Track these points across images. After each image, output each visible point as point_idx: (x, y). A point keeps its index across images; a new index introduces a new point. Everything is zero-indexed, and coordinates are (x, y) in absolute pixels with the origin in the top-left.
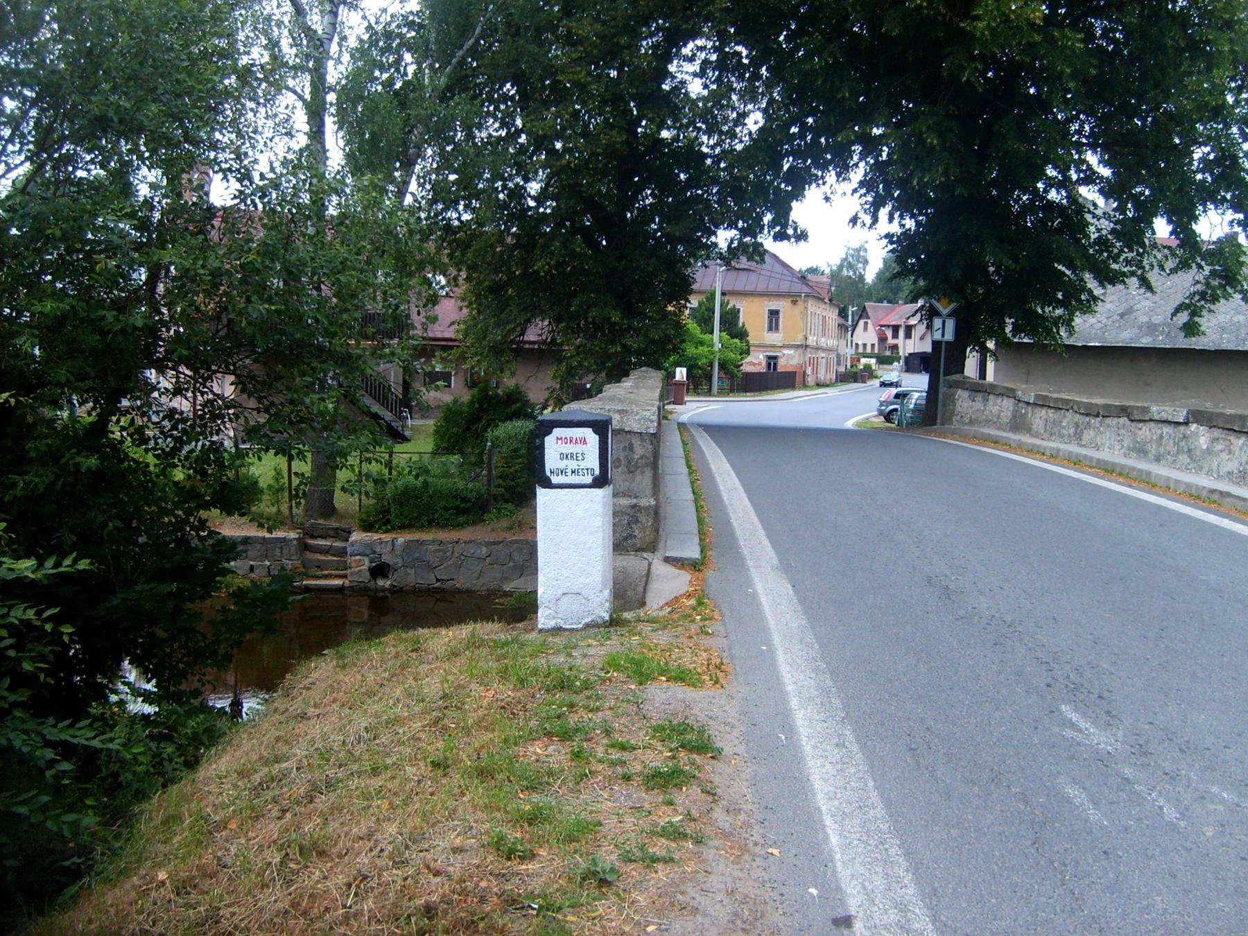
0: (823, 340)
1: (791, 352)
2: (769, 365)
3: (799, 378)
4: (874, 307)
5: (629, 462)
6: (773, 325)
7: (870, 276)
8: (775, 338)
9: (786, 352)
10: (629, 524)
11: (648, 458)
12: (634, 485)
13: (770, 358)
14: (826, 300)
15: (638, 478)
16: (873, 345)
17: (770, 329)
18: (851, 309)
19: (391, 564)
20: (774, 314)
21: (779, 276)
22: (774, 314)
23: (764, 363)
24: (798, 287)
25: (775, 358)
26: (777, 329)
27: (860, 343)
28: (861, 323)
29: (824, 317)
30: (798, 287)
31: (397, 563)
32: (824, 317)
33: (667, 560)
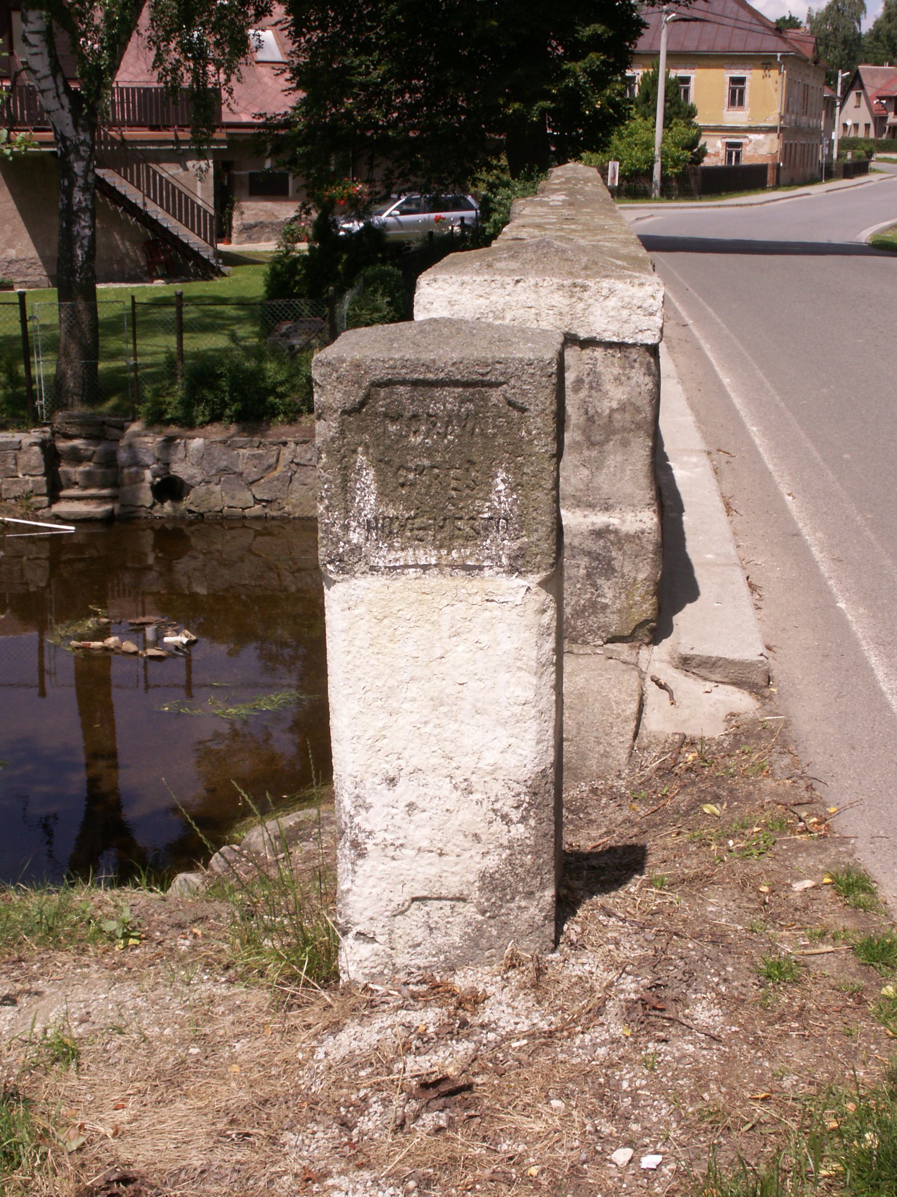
0: (804, 119)
1: (760, 137)
2: (730, 155)
3: (770, 175)
4: (871, 72)
5: (590, 420)
6: (736, 97)
7: (866, 25)
8: (738, 117)
9: (753, 137)
10: (589, 576)
11: (638, 410)
12: (602, 479)
13: (729, 145)
14: (810, 63)
15: (613, 460)
16: (867, 126)
17: (732, 103)
18: (842, 75)
19: (185, 477)
20: (738, 81)
21: (747, 26)
22: (738, 81)
23: (723, 153)
24: (771, 43)
25: (739, 145)
26: (741, 103)
27: (849, 123)
28: (853, 95)
29: (806, 87)
30: (771, 43)
31: (193, 477)
32: (806, 87)
33: (685, 663)
